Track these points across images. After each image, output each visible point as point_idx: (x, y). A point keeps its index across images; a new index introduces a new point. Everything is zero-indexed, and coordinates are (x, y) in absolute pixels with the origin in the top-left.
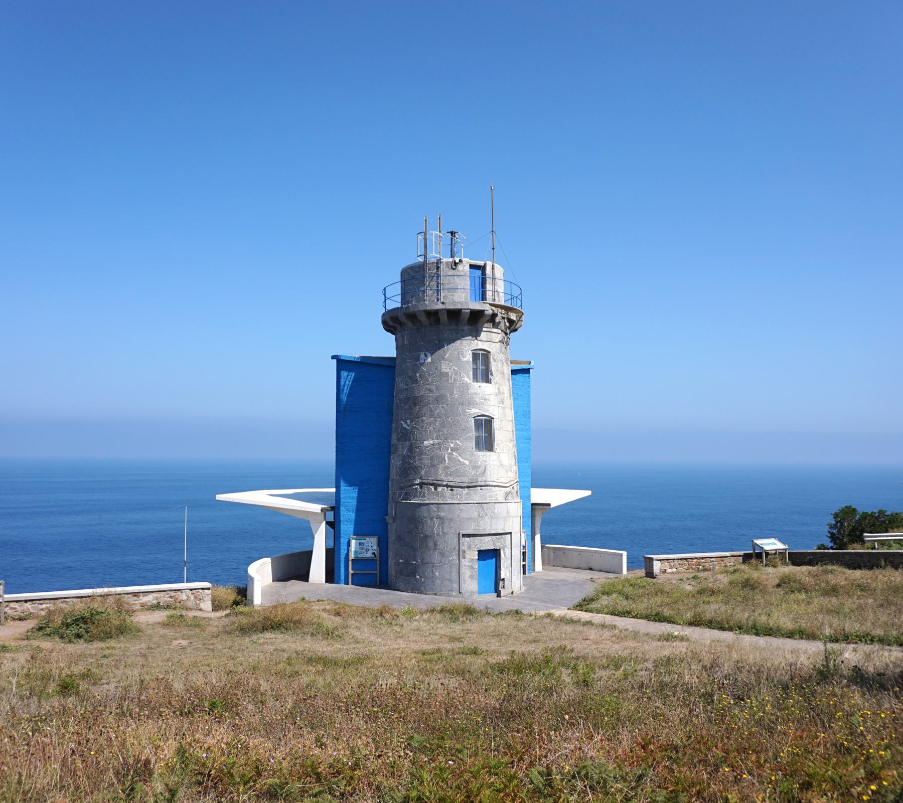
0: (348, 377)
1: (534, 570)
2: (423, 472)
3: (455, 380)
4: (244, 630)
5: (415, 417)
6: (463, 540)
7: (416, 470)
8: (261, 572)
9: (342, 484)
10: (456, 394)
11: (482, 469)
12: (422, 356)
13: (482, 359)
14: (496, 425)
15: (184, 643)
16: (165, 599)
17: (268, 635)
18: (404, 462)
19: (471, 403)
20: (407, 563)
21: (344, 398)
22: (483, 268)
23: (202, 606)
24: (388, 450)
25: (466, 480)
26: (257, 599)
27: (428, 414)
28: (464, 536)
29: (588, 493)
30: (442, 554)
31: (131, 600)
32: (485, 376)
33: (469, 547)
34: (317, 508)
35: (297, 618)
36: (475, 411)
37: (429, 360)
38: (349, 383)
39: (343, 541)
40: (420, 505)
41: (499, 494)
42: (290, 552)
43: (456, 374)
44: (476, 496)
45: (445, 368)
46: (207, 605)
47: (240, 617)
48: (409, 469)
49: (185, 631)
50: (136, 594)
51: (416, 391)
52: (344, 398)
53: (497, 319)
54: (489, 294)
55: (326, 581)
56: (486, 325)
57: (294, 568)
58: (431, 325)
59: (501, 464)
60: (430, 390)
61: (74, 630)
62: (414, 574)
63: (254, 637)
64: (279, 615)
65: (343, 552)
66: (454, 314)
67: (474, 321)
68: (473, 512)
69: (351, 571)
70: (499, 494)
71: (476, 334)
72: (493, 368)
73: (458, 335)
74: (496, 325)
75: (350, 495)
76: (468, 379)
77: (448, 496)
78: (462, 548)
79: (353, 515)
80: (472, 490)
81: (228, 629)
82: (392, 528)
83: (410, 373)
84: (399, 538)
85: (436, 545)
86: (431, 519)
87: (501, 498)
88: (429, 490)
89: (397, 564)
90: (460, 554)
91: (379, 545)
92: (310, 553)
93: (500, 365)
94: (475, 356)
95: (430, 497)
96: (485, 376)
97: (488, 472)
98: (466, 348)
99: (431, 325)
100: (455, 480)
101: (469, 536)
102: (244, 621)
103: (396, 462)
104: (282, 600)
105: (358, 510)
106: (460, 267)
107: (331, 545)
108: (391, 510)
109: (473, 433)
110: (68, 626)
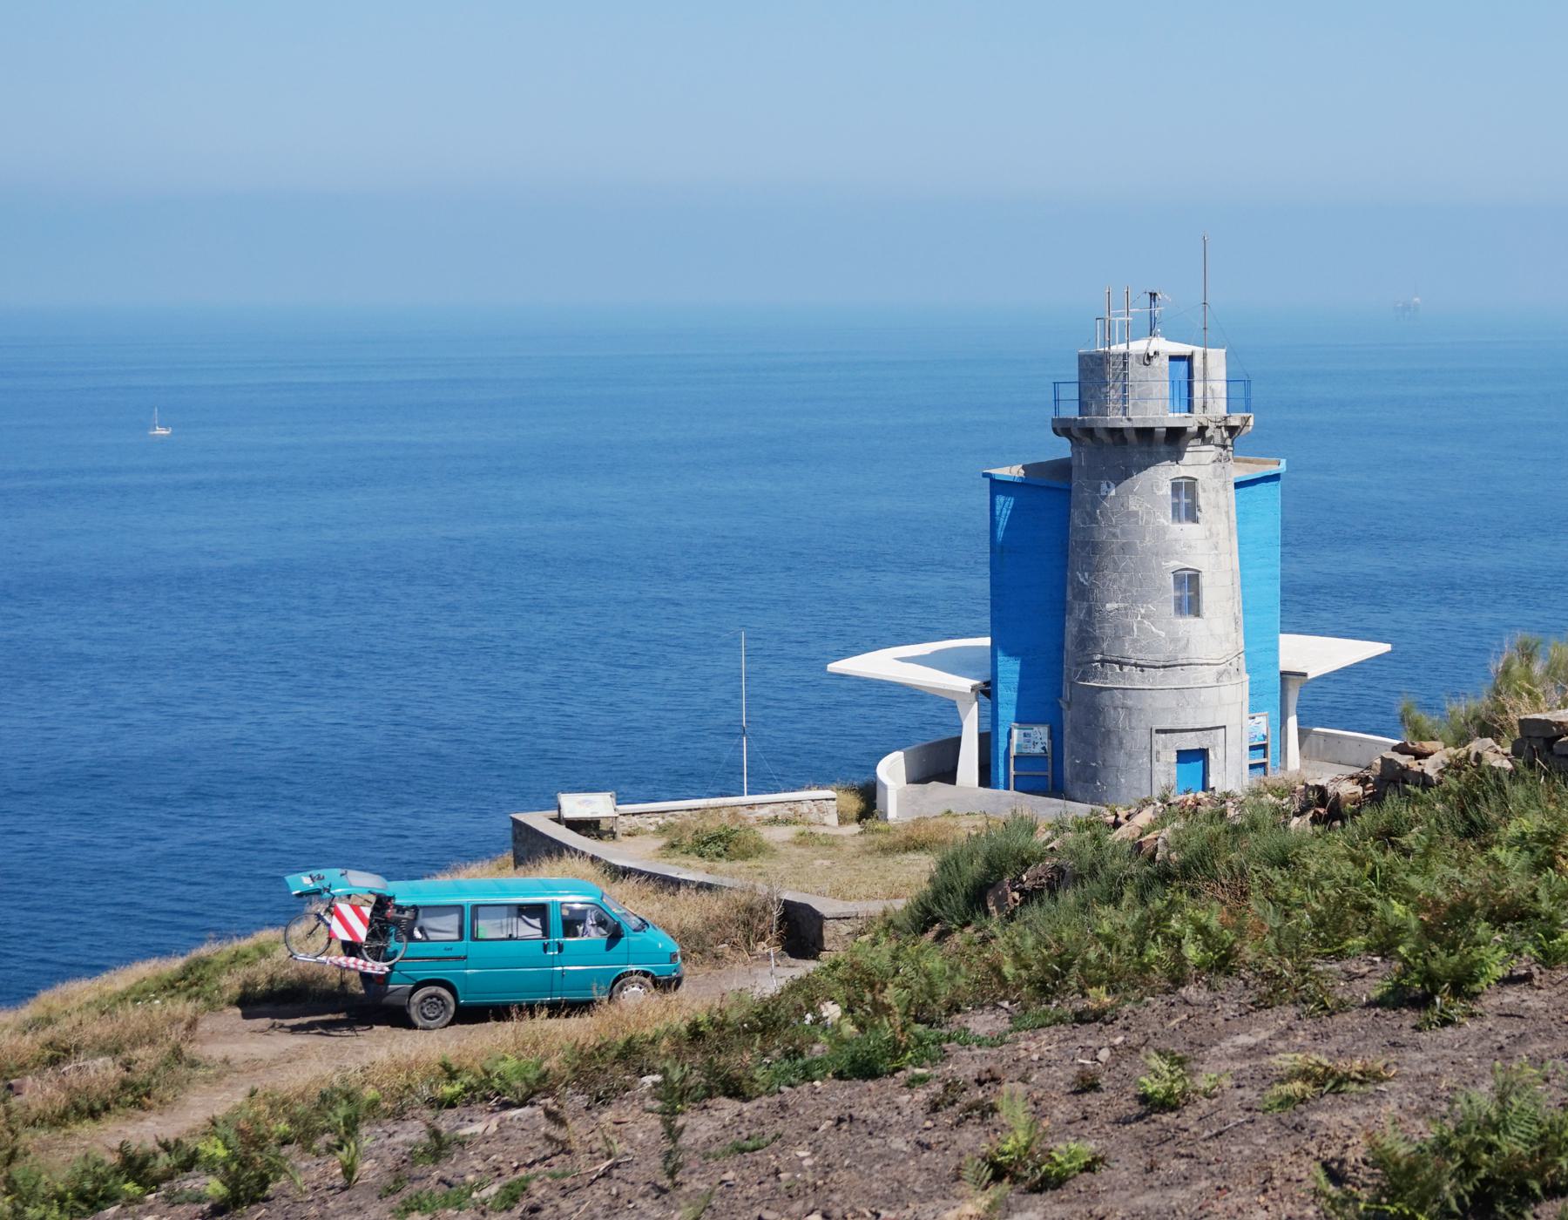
0: (1005, 504)
1: (1285, 768)
2: (1105, 646)
3: (1147, 523)
4: (886, 851)
5: (1095, 570)
6: (1157, 737)
7: (1096, 641)
8: (892, 770)
9: (1001, 658)
10: (1148, 541)
11: (1183, 643)
12: (1104, 486)
13: (1186, 490)
14: (1204, 581)
15: (827, 863)
16: (783, 812)
17: (911, 856)
18: (1081, 630)
19: (1169, 554)
20: (1085, 765)
21: (1000, 534)
22: (1189, 359)
23: (827, 820)
24: (1062, 609)
25: (1161, 658)
26: (892, 812)
27: (1111, 566)
28: (1158, 731)
29: (1386, 647)
30: (1130, 755)
31: (744, 812)
32: (1192, 514)
33: (1165, 747)
34: (964, 684)
35: (943, 837)
36: (1175, 564)
37: (1113, 493)
38: (1006, 512)
39: (1003, 731)
40: (1101, 689)
41: (1208, 675)
42: (933, 740)
43: (1148, 513)
44: (1175, 678)
45: (1133, 505)
46: (832, 819)
47: (879, 836)
48: (1087, 640)
49: (823, 850)
50: (751, 806)
51: (1096, 534)
52: (1000, 534)
53: (1208, 434)
54: (1198, 403)
55: (981, 784)
56: (1192, 442)
57: (936, 766)
58: (1115, 444)
59: (1215, 634)
60: (1114, 535)
61: (713, 848)
62: (1093, 779)
63: (898, 858)
64: (922, 834)
65: (1002, 745)
66: (1146, 433)
67: (1175, 440)
68: (1170, 700)
69: (1012, 772)
70: (1208, 675)
71: (1177, 456)
72: (1202, 501)
73: (1154, 460)
74: (1206, 441)
75: (1010, 670)
76: (1164, 518)
77: (1136, 679)
78: (1155, 748)
79: (1014, 696)
80: (1169, 671)
81: (869, 848)
82: (1067, 715)
83: (1088, 507)
84: (1075, 729)
85: (1121, 743)
86: (1115, 708)
87: (1211, 681)
88: (1113, 669)
89: (1073, 765)
90: (1152, 755)
91: (1051, 737)
92: (957, 742)
93: (1212, 496)
94: (1175, 487)
95: (1112, 679)
96: (1192, 514)
97: (1192, 646)
98: (1162, 476)
99: (1115, 444)
100: (1148, 658)
101: (1165, 731)
102: (885, 840)
103: (1071, 628)
104: (926, 812)
105: (1022, 689)
106: (1155, 362)
107: (987, 728)
108: (1066, 693)
109: (1172, 594)
110: (705, 844)
